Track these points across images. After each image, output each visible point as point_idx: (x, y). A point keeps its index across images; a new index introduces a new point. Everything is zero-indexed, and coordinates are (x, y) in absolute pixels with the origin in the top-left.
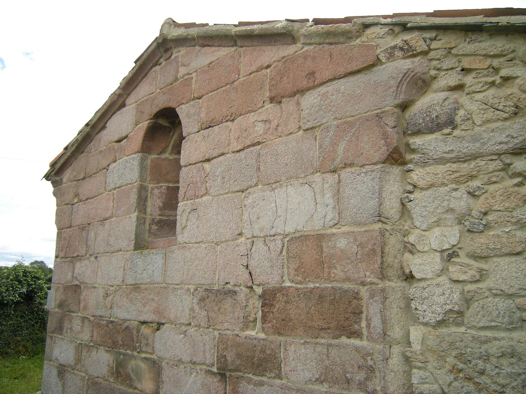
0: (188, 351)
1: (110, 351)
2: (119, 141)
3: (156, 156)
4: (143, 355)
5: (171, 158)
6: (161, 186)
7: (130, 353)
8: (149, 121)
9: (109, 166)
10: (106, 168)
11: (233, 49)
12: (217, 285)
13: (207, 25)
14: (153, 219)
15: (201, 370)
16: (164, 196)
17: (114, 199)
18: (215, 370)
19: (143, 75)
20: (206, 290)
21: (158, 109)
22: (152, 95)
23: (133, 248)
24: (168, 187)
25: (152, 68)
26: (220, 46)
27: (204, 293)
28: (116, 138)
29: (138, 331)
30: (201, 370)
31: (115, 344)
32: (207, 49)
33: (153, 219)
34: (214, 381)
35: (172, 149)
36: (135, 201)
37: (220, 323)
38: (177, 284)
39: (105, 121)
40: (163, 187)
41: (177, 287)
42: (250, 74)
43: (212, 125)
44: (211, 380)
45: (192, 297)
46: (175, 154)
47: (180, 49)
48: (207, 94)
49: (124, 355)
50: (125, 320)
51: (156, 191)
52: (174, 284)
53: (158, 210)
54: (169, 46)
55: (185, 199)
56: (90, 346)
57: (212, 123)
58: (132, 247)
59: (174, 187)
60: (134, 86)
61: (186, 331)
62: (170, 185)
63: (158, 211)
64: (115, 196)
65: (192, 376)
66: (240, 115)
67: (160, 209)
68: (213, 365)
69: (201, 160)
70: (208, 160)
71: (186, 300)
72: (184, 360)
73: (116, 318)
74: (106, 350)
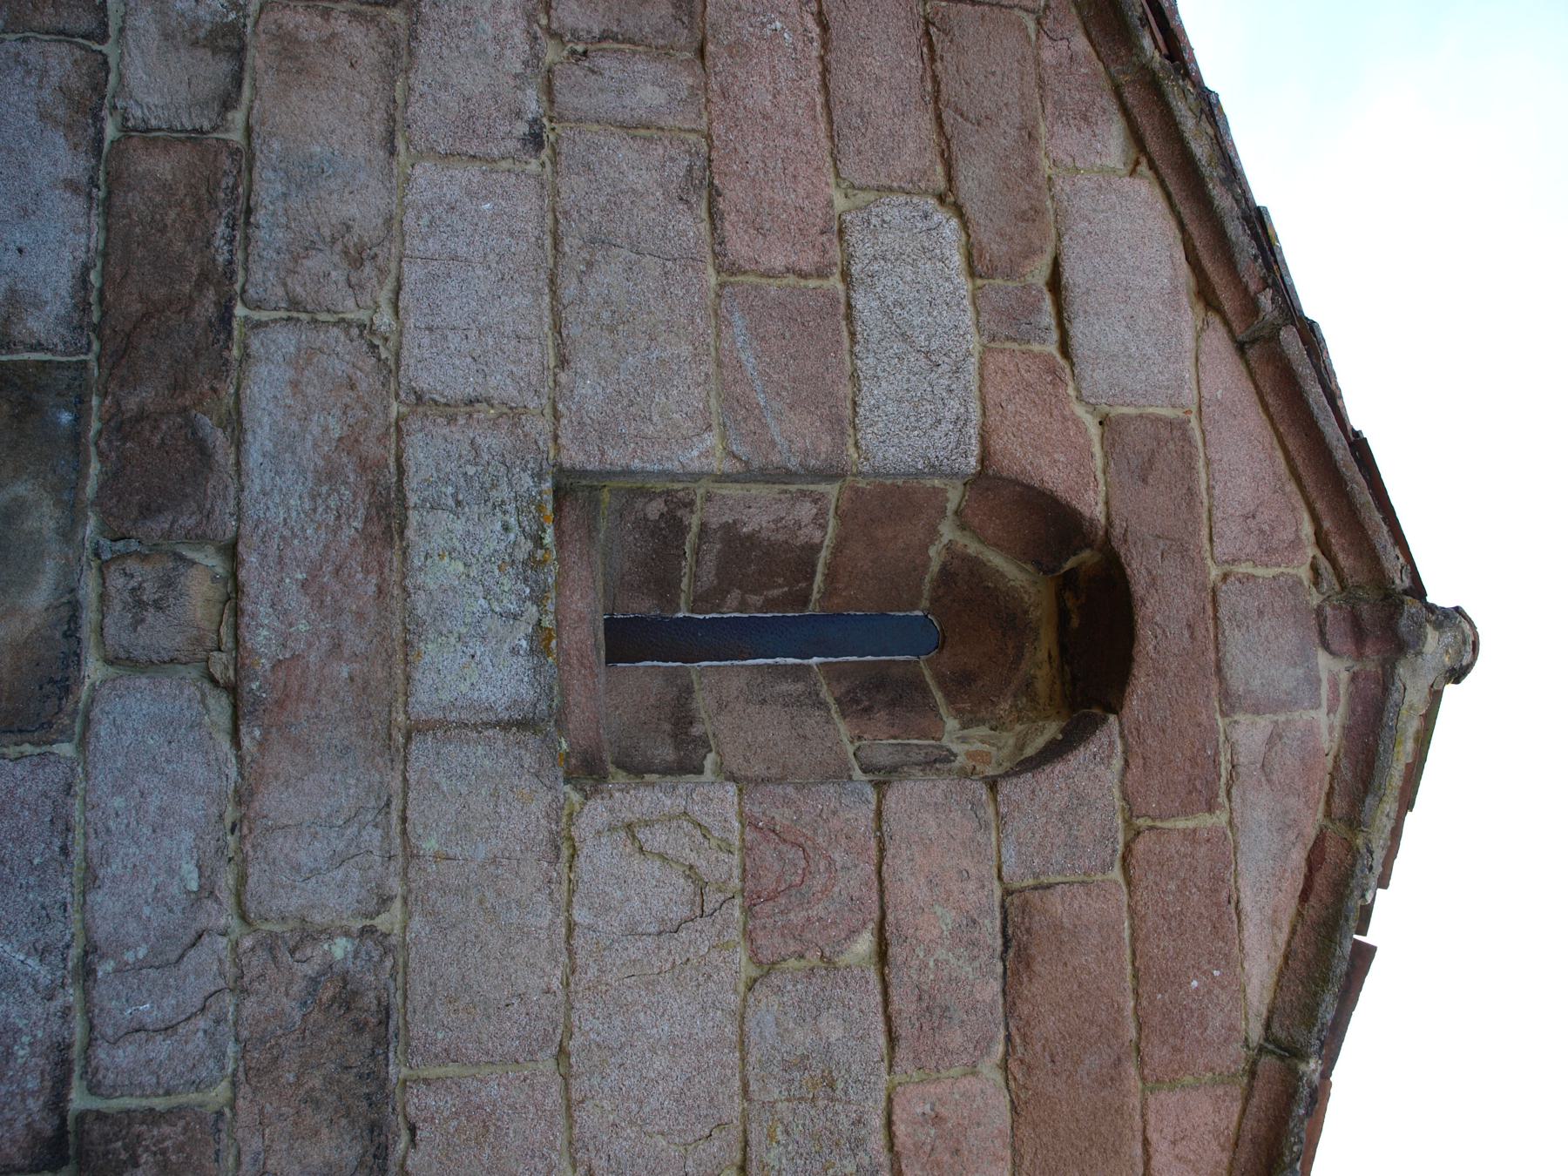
0: (132, 925)
1: (85, 307)
2: (1056, 284)
3: (951, 506)
4: (89, 589)
5: (932, 552)
6: (823, 527)
7: (91, 488)
8: (1103, 521)
9: (959, 211)
10: (948, 198)
11: (1256, 1033)
12: (405, 1071)
13: (1384, 882)
14: (690, 505)
15: (66, 1012)
16: (781, 537)
17: (803, 275)
18: (78, 1099)
19: (1299, 461)
20: (386, 1012)
21: (1139, 588)
22: (1205, 532)
23: (567, 464)
24: (815, 549)
25: (1316, 519)
26: (1286, 958)
27: (370, 999)
28: (1073, 274)
29: (198, 539)
30: (66, 1012)
31: (121, 355)
32: (1298, 857)
33: (692, 503)
34: (30, 1102)
35: (966, 558)
36: (776, 458)
37: (261, 1112)
38: (404, 820)
39: (1165, 170)
40: (818, 534)
41: (395, 816)
42: (1146, 1142)
43: (1011, 953)
44: (32, 1084)
45: (357, 924)
46: (944, 567)
47: (1342, 709)
48: (1132, 912)
49: (76, 437)
50: (235, 424)
51: (806, 511)
52: (406, 794)
53: (728, 518)
54: (1368, 651)
55: (750, 835)
56: (98, 119)
57: (1018, 955)
58: (573, 457)
59: (814, 566)
60: (1270, 400)
61: (217, 900)
62: (824, 555)
63: (724, 519)
64: (812, 283)
65: (33, 962)
66: (1014, 1108)
67: (726, 527)
68: (93, 1089)
69: (890, 918)
70: (882, 954)
71: (342, 885)
72: (96, 897)
73: (246, 355)
74: (86, 269)
